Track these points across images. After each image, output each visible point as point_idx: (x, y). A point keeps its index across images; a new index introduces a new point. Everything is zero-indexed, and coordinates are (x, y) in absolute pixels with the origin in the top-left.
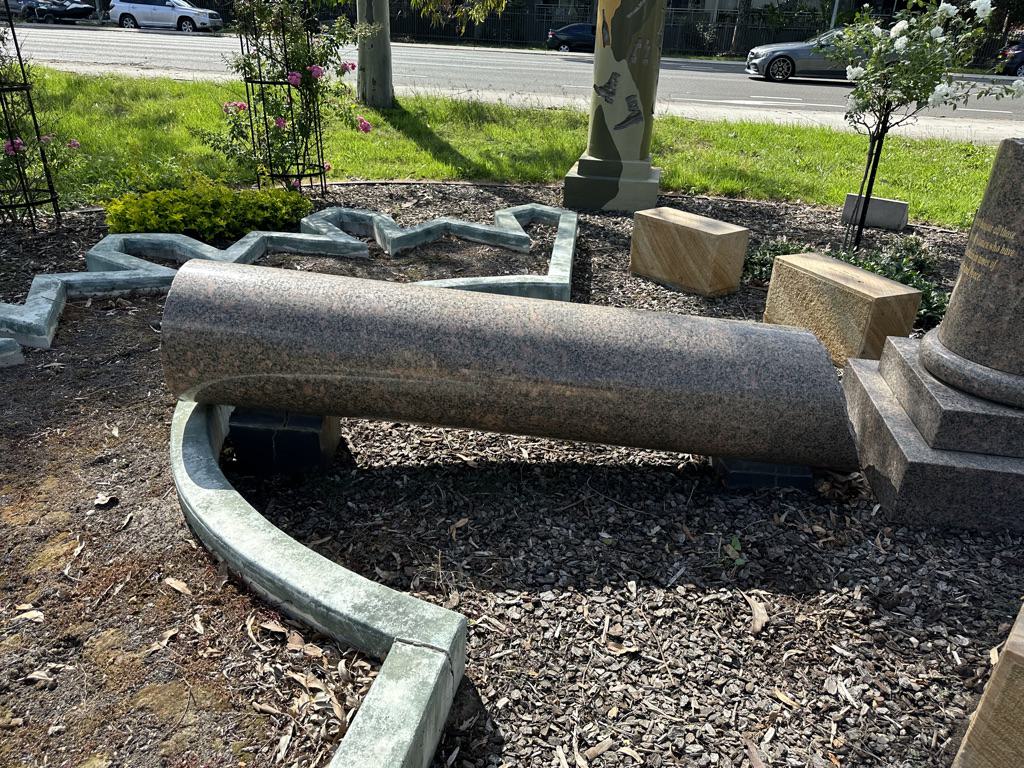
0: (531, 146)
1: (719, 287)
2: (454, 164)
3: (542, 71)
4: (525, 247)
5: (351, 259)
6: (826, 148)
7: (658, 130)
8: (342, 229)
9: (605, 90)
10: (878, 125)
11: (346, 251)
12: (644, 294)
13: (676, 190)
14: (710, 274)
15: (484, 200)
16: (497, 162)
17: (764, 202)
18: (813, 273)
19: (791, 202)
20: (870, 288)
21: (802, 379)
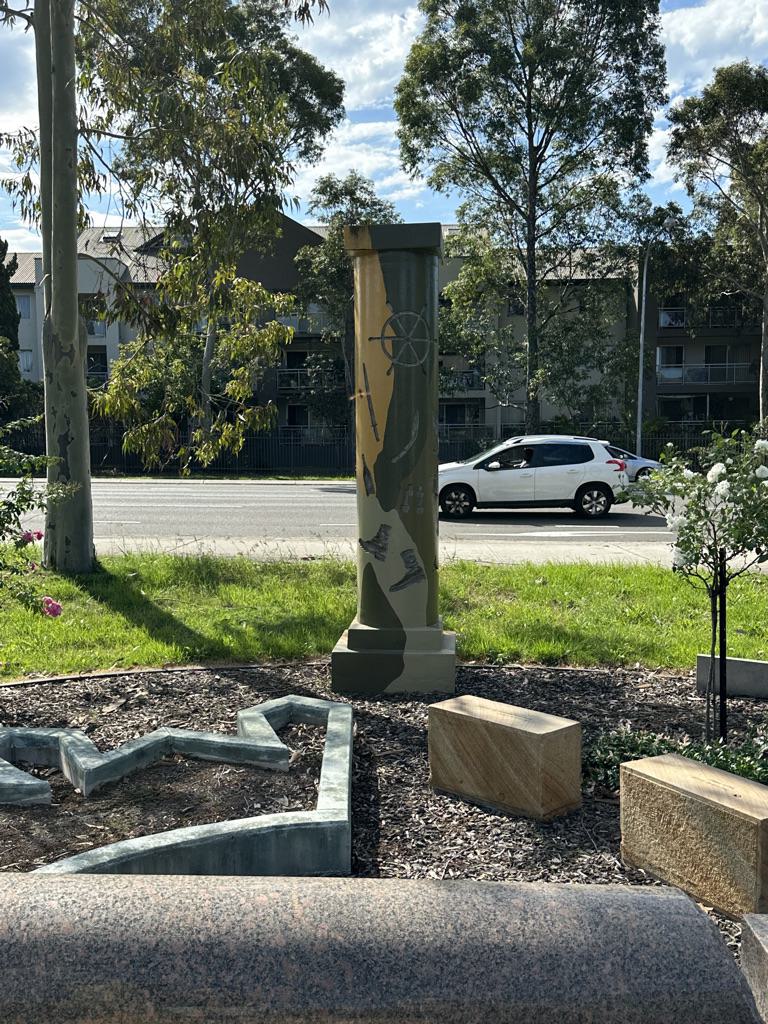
0: (284, 611)
1: (555, 805)
2: (178, 643)
3: (293, 507)
4: (281, 762)
5: (24, 808)
6: (658, 592)
7: (446, 580)
8: (13, 763)
9: (373, 544)
10: (715, 577)
11: (16, 796)
12: (454, 822)
13: (478, 659)
14: (539, 788)
15: (222, 691)
16: (239, 634)
17: (594, 669)
18: (674, 787)
19: (628, 667)
20: (750, 806)
21: (686, 971)
